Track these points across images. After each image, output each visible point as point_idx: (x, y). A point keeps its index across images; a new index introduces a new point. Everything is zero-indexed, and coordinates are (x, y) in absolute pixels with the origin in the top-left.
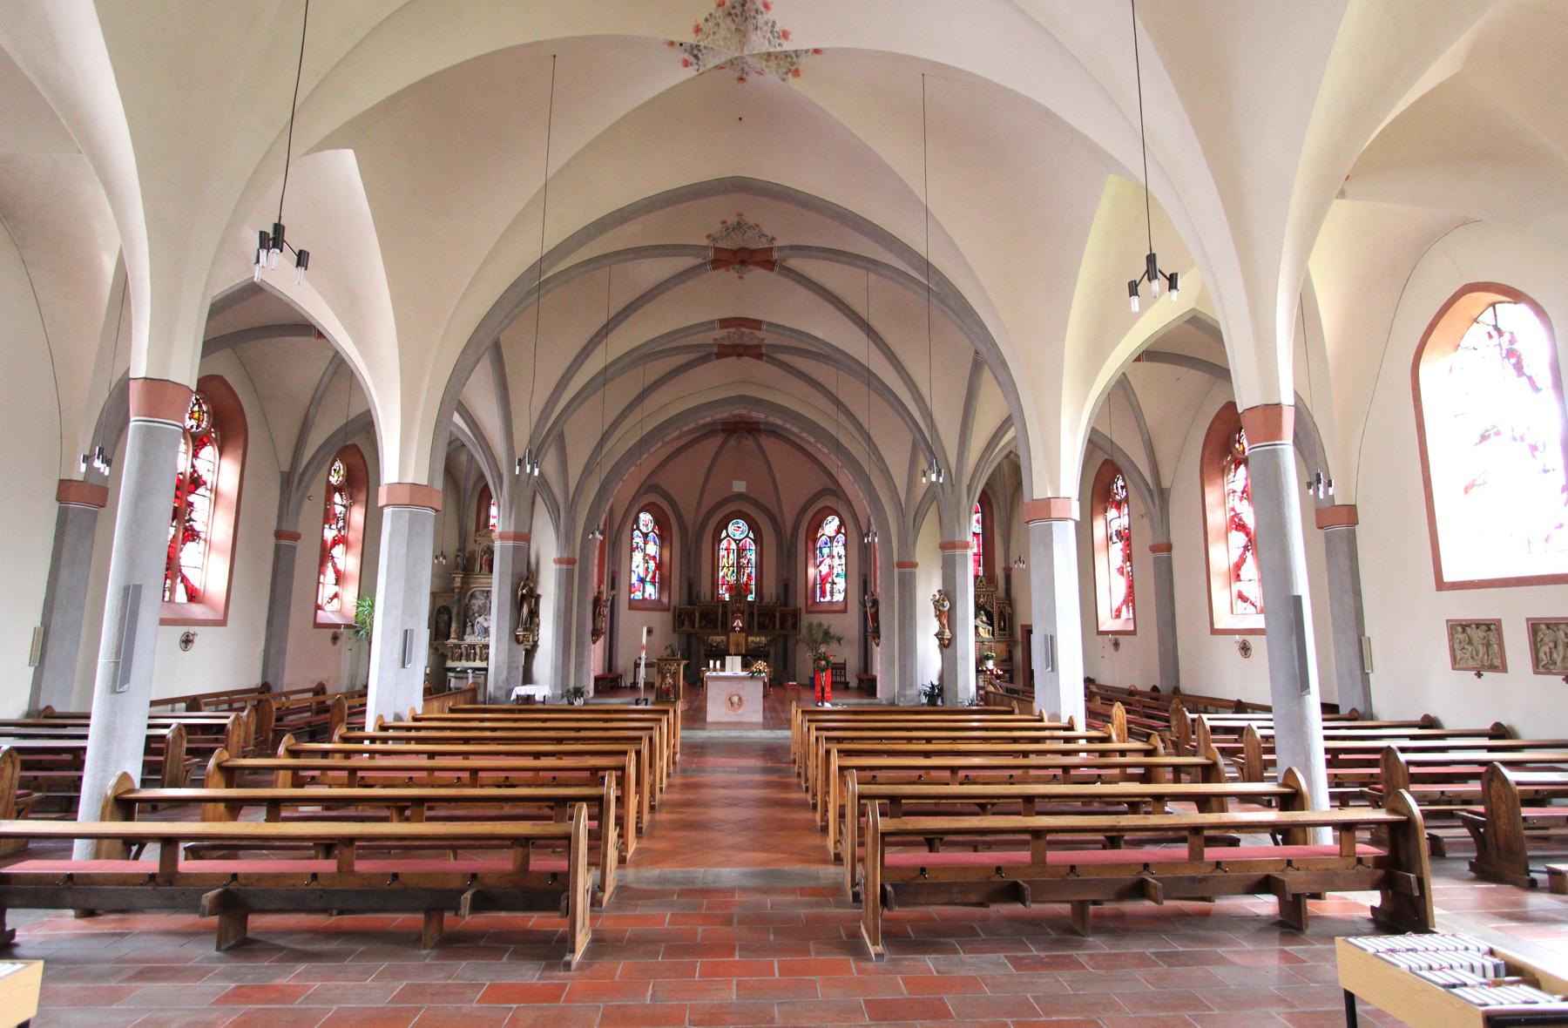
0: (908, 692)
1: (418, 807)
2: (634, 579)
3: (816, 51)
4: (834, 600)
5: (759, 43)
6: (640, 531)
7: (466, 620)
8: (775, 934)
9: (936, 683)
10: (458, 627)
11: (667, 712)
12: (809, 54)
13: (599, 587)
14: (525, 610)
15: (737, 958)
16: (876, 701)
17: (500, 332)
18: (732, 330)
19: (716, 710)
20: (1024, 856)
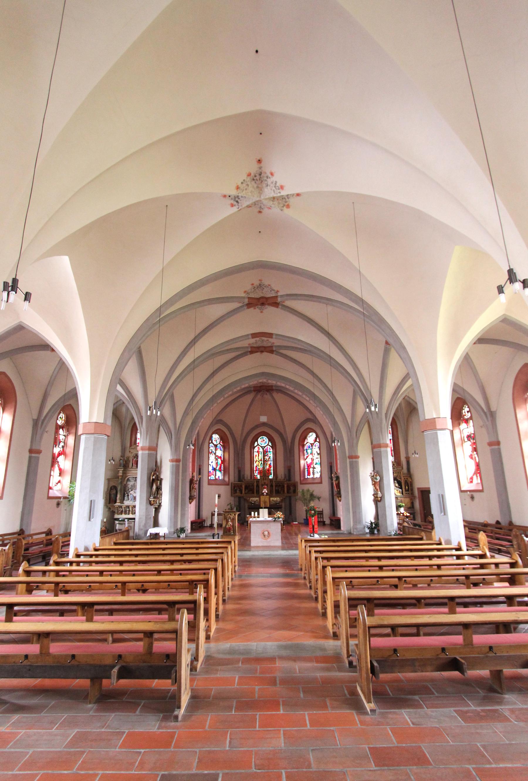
0: (358, 527)
1: (91, 608)
2: (211, 469)
3: (298, 195)
4: (315, 477)
5: (269, 192)
7: (125, 493)
8: (304, 692)
9: (373, 521)
10: (121, 497)
11: (230, 542)
12: (294, 196)
13: (193, 474)
14: (154, 487)
15: (282, 712)
17: (141, 344)
18: (258, 339)
19: (256, 540)
20: (459, 639)
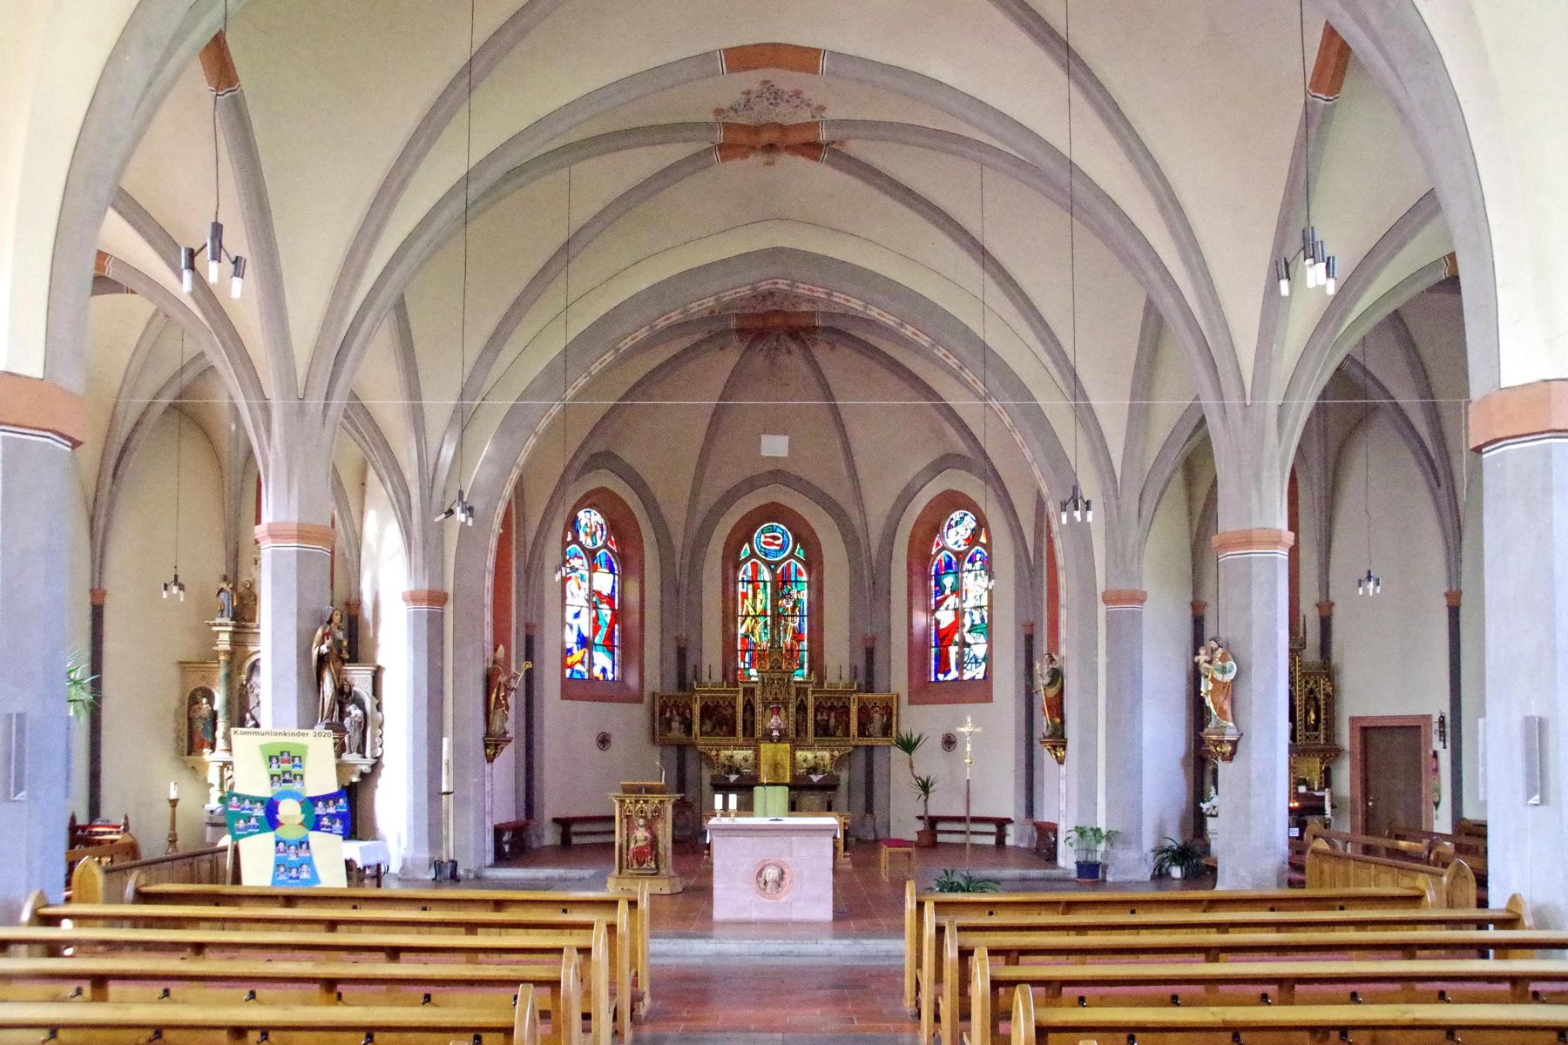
2: (571, 639)
4: (967, 676)
6: (580, 544)
16: (1054, 873)
